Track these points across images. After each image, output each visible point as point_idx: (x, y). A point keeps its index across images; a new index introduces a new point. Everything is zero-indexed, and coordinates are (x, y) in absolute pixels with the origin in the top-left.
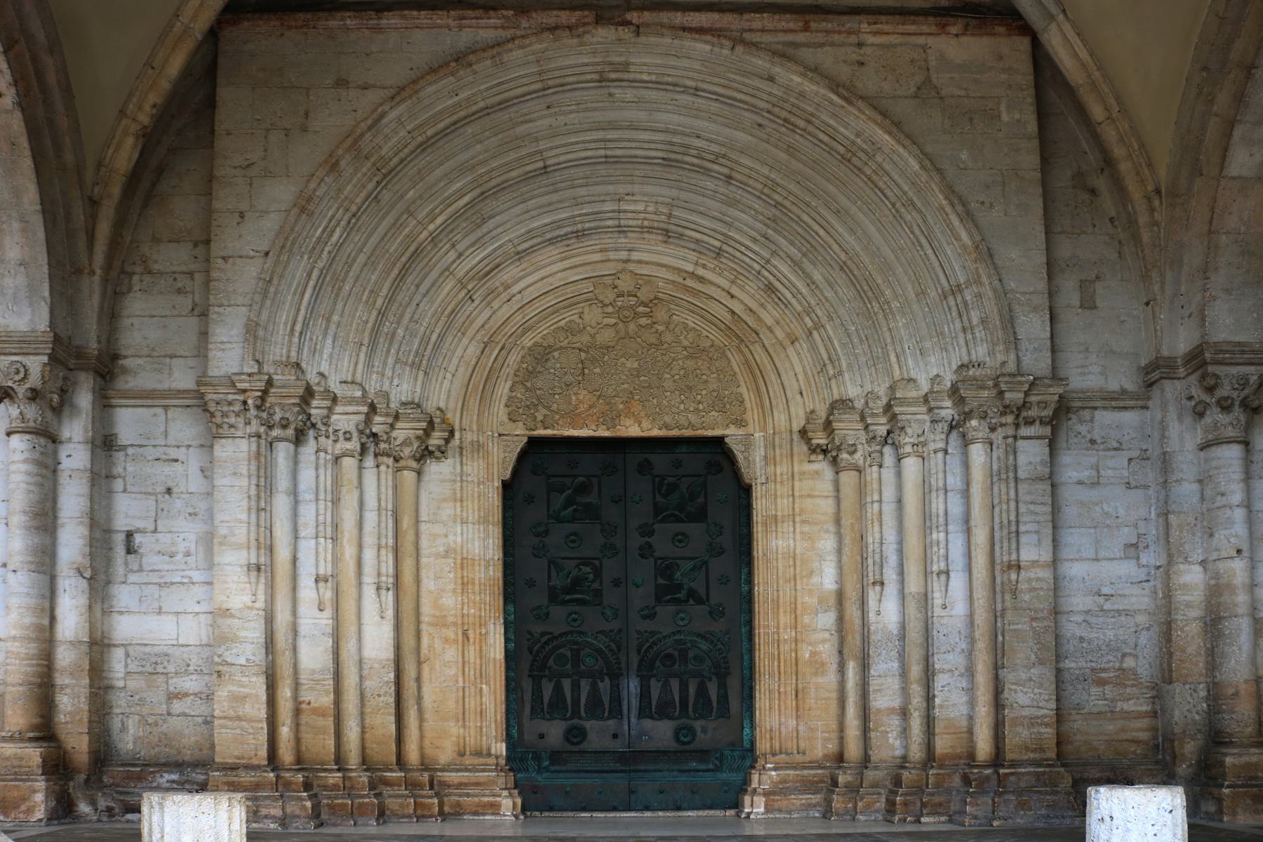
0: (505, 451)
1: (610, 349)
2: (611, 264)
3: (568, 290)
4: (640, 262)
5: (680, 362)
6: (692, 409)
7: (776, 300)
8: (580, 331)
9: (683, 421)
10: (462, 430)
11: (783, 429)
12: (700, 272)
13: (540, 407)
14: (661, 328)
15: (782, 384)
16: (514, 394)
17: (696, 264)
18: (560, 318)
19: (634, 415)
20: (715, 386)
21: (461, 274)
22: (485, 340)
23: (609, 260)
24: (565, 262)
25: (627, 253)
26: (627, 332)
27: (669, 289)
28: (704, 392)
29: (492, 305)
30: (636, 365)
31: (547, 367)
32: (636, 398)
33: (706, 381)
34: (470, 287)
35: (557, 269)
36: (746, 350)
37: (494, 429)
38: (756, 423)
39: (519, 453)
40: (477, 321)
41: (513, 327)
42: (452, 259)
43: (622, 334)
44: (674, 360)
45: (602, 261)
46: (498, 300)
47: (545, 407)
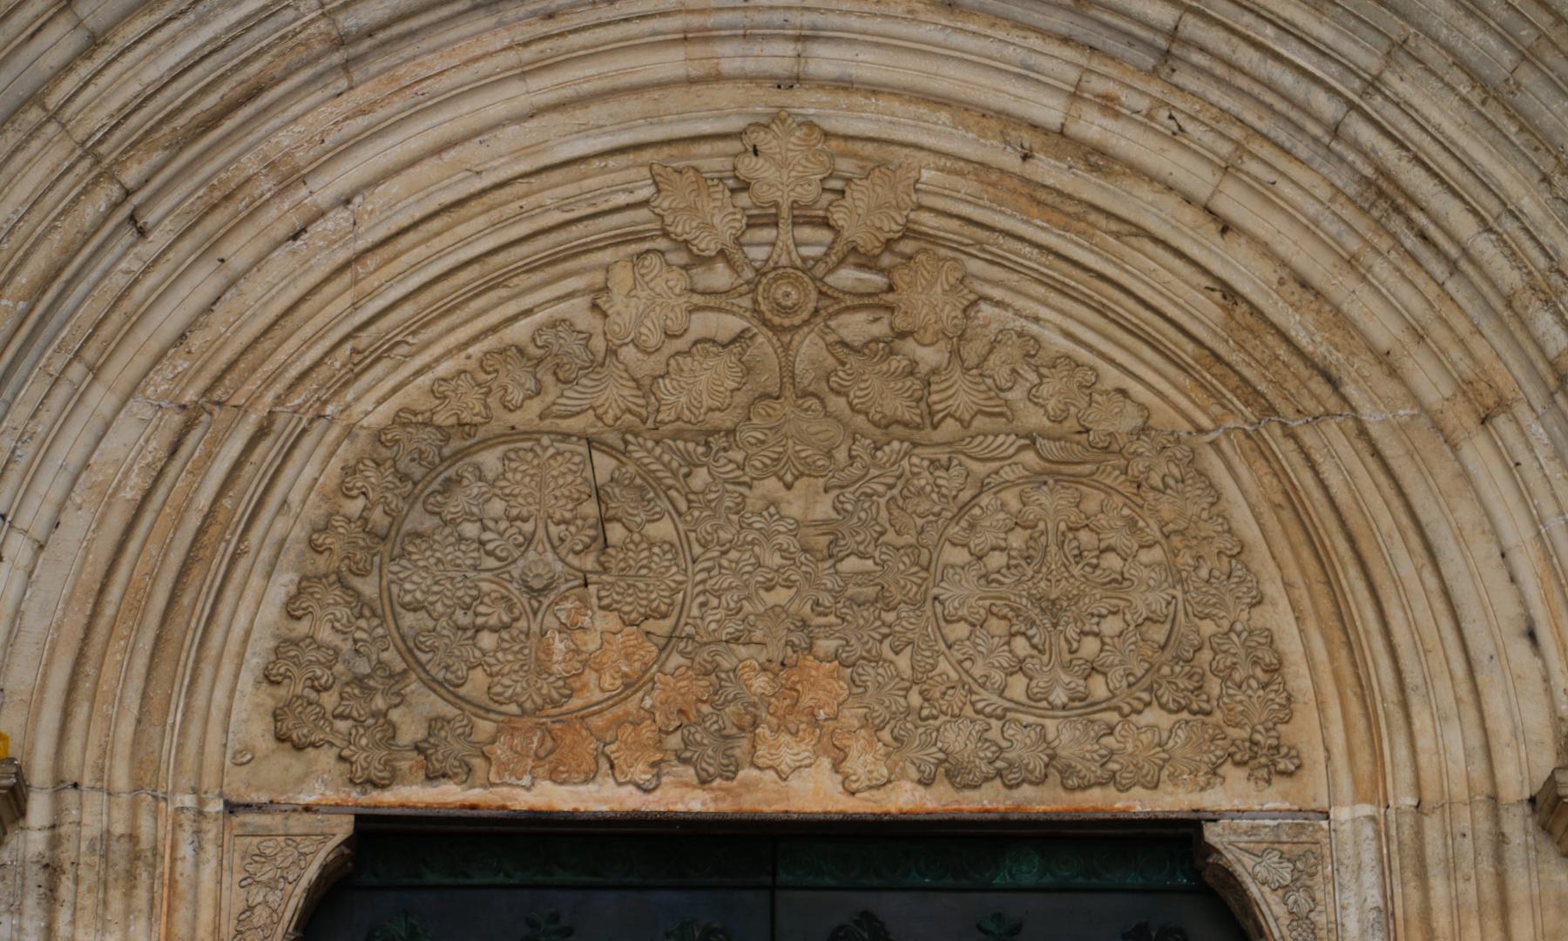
0: (249, 881)
1: (718, 442)
2: (723, 95)
3: (547, 198)
4: (844, 85)
5: (1011, 498)
6: (1059, 696)
7: (1411, 241)
8: (594, 365)
9: (1021, 747)
10: (60, 785)
11: (1459, 790)
12: (1092, 126)
13: (413, 686)
14: (929, 356)
15: (1446, 593)
16: (302, 628)
17: (1076, 95)
18: (511, 309)
19: (814, 722)
20: (1157, 600)
21: (100, 117)
22: (190, 396)
23: (717, 78)
24: (534, 83)
25: (790, 49)
26: (788, 373)
27: (965, 194)
28: (1111, 626)
29: (226, 250)
30: (823, 508)
31: (450, 510)
32: (826, 645)
33: (1120, 581)
34: (131, 175)
35: (502, 110)
36: (1285, 450)
37: (209, 781)
38: (1340, 760)
39: (312, 890)
40: (157, 316)
41: (310, 342)
42: (55, 59)
43: (768, 379)
44: (983, 487)
45: (691, 81)
46: (248, 231)
47: (432, 684)
